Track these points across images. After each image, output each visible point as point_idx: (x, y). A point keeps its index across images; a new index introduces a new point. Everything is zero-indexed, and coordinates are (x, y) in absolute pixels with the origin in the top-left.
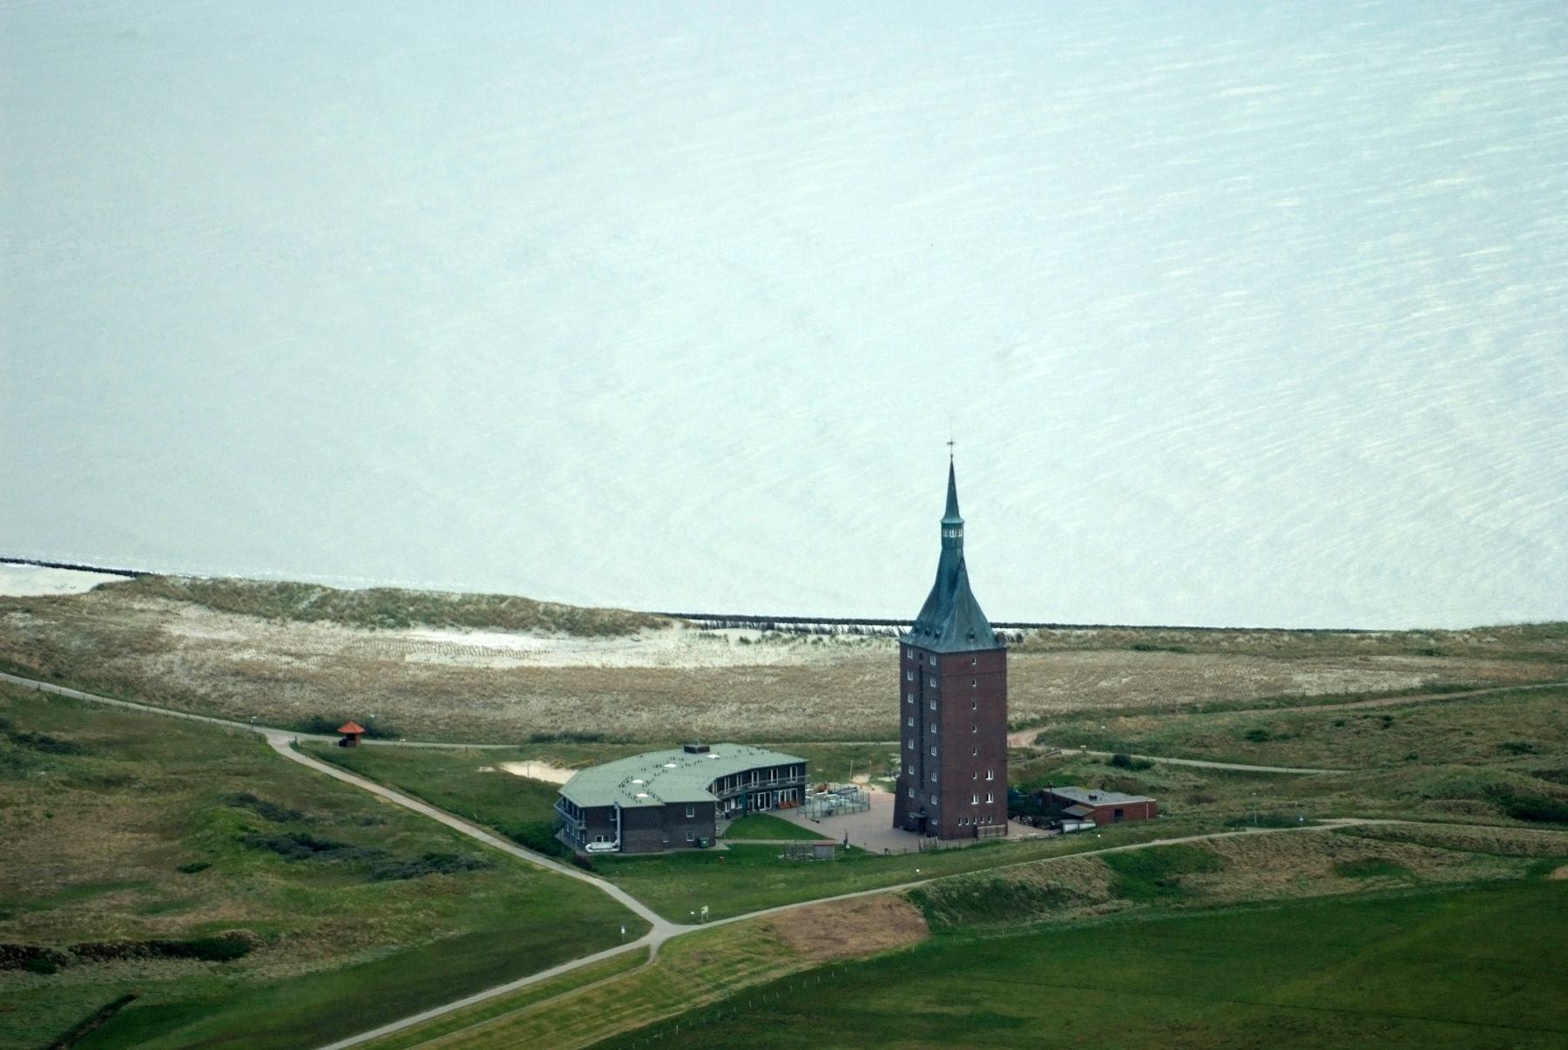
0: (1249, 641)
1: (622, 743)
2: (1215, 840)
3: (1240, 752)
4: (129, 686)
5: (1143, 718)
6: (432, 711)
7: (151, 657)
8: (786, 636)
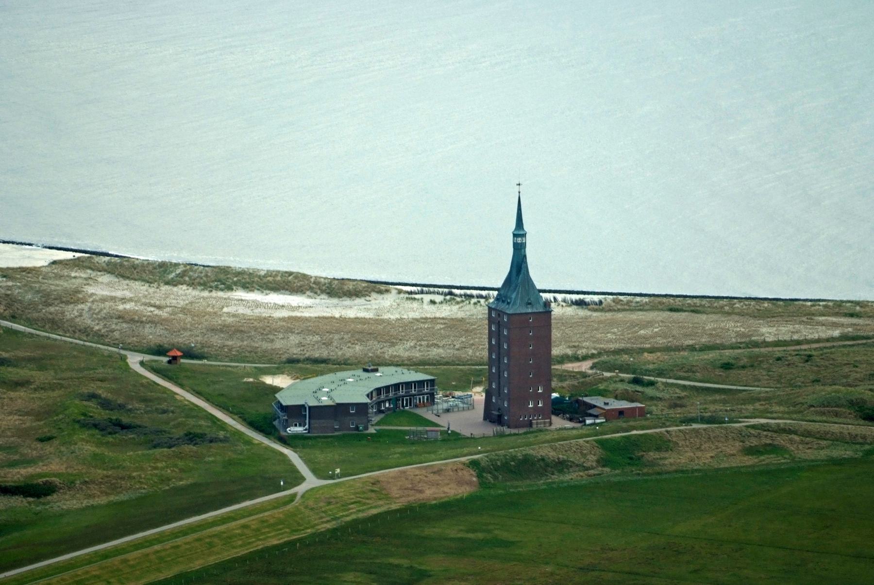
0: (742, 307)
1: (339, 365)
2: (670, 431)
3: (713, 375)
4: (55, 324)
5: (659, 354)
6: (230, 343)
7: (71, 306)
8: (459, 299)
